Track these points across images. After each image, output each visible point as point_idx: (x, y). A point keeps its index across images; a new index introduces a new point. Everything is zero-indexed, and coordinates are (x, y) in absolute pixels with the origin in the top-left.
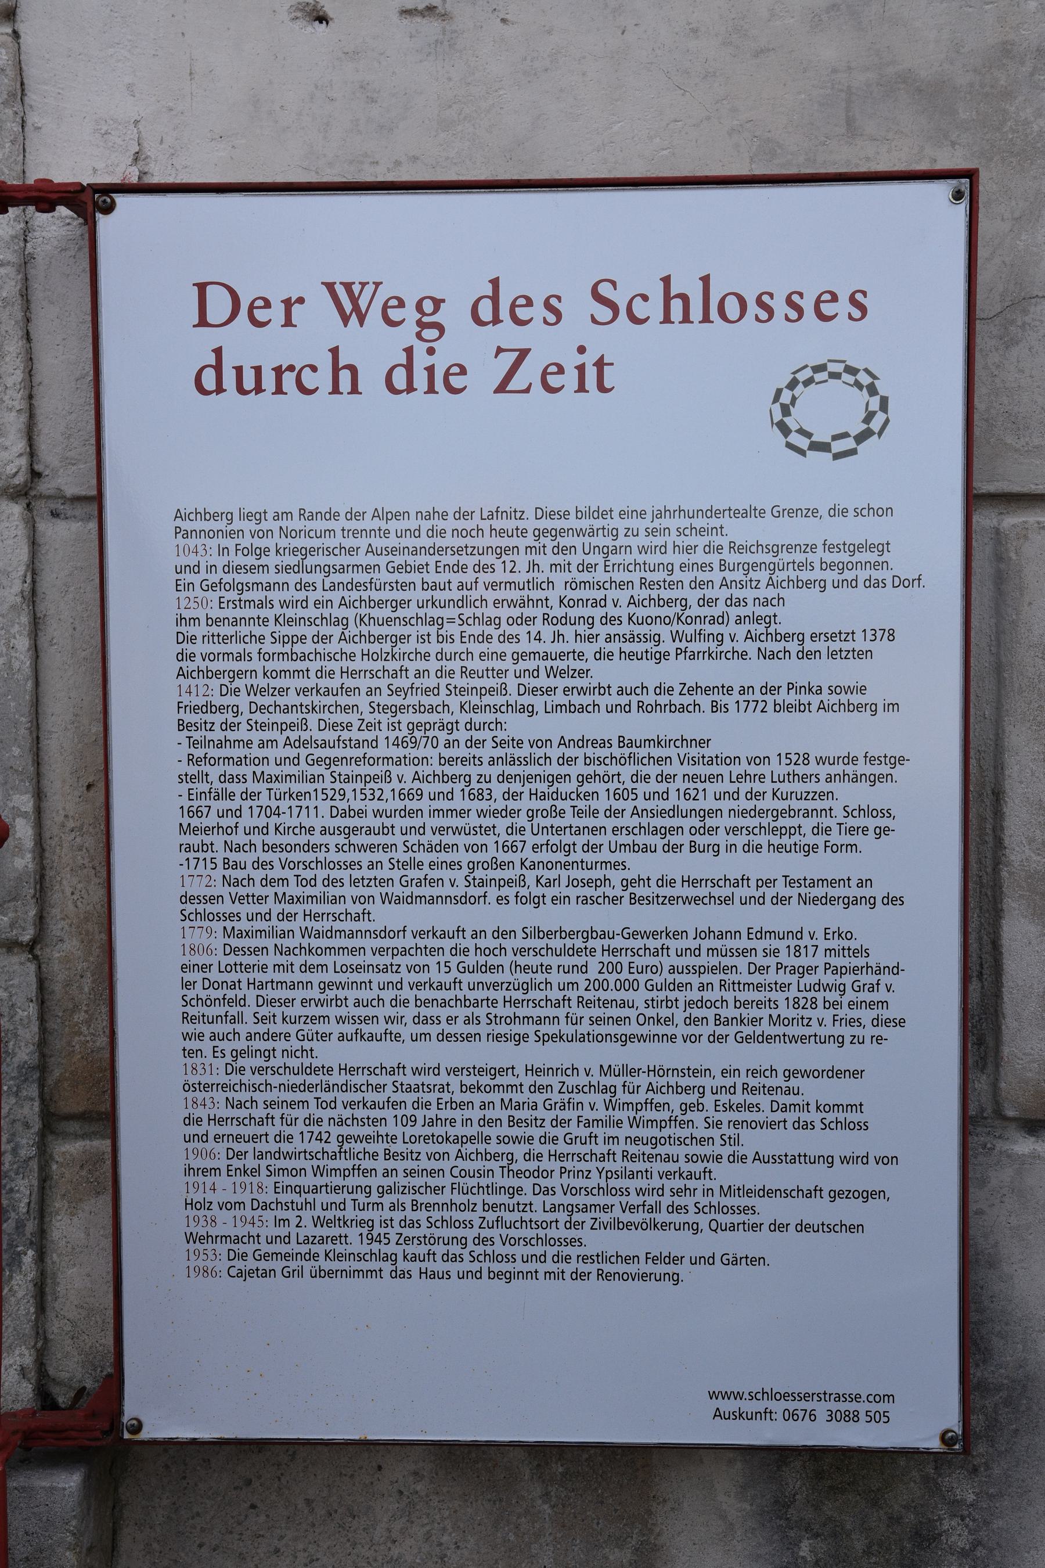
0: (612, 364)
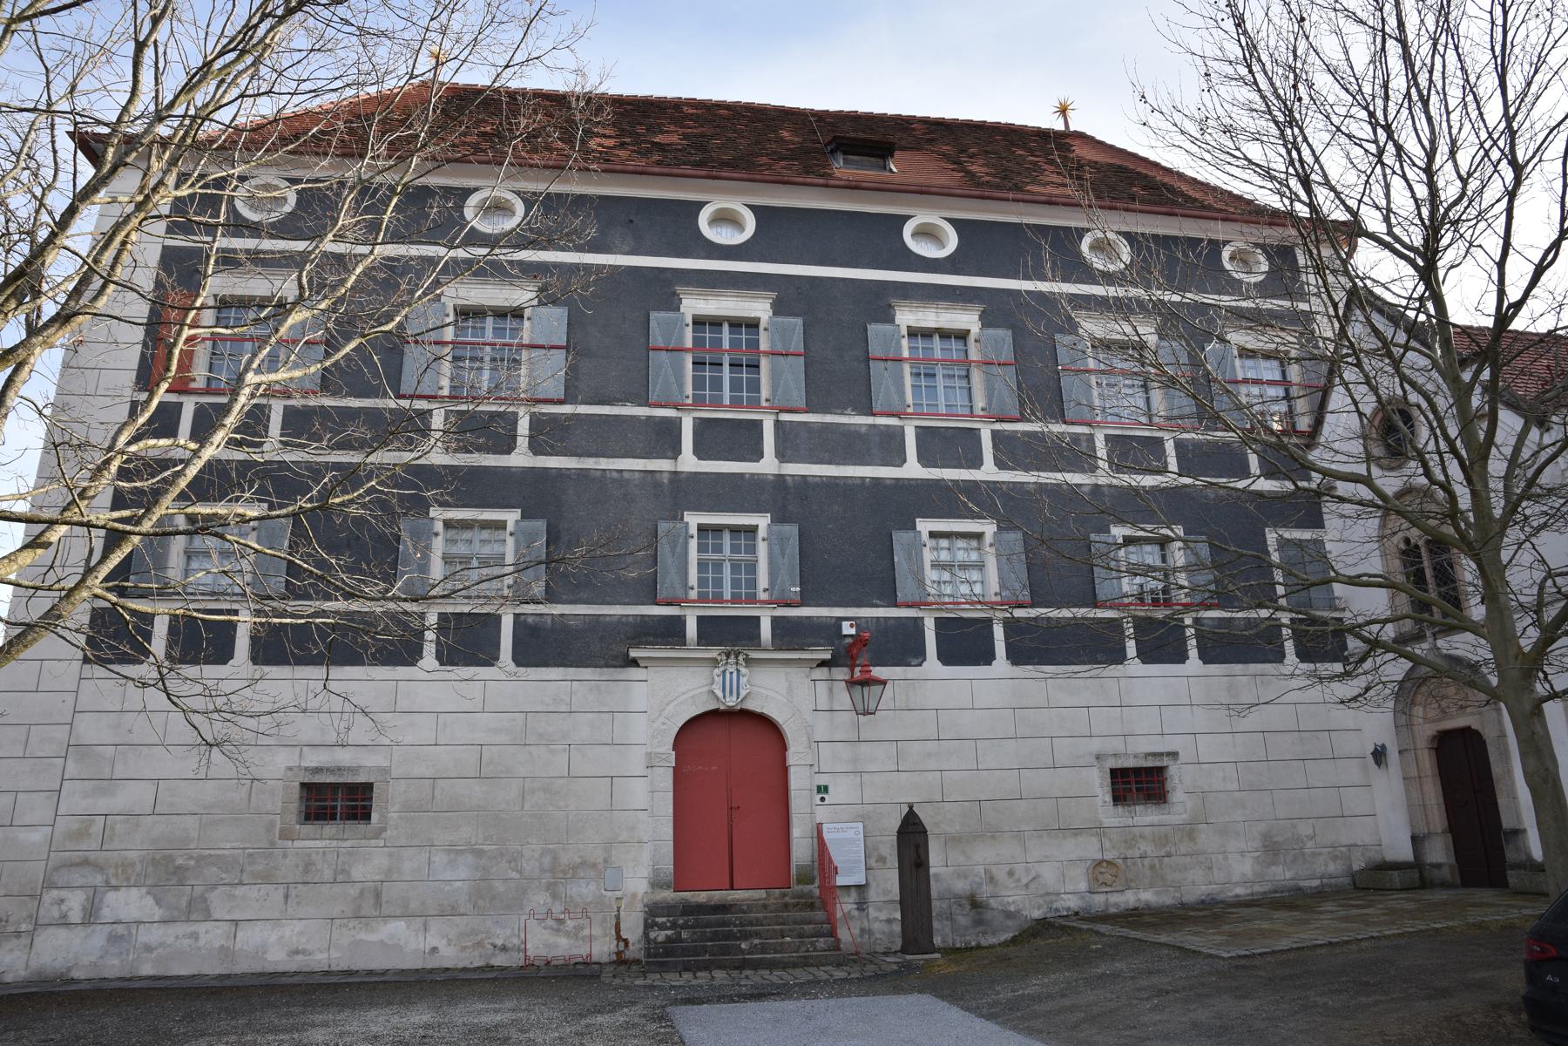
0: (912, 833)
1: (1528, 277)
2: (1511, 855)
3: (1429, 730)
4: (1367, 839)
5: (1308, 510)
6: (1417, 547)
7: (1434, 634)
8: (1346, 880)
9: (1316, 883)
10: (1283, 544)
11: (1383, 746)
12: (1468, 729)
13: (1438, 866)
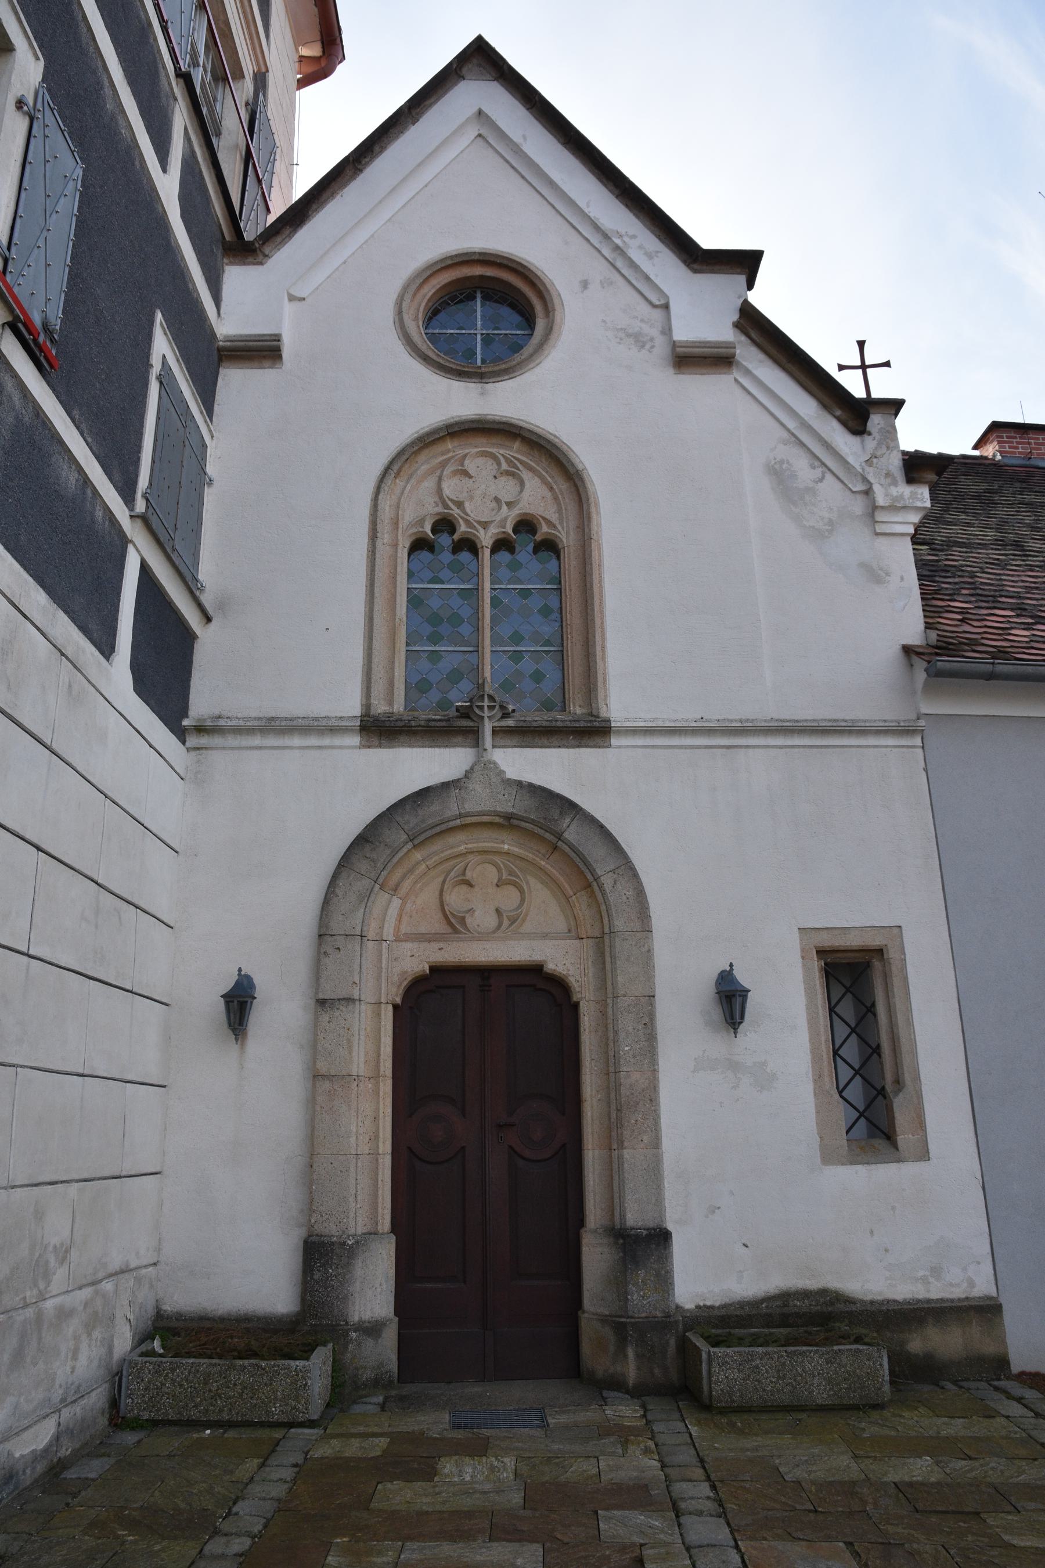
3: (415, 960)
12: (536, 970)
13: (373, 1329)
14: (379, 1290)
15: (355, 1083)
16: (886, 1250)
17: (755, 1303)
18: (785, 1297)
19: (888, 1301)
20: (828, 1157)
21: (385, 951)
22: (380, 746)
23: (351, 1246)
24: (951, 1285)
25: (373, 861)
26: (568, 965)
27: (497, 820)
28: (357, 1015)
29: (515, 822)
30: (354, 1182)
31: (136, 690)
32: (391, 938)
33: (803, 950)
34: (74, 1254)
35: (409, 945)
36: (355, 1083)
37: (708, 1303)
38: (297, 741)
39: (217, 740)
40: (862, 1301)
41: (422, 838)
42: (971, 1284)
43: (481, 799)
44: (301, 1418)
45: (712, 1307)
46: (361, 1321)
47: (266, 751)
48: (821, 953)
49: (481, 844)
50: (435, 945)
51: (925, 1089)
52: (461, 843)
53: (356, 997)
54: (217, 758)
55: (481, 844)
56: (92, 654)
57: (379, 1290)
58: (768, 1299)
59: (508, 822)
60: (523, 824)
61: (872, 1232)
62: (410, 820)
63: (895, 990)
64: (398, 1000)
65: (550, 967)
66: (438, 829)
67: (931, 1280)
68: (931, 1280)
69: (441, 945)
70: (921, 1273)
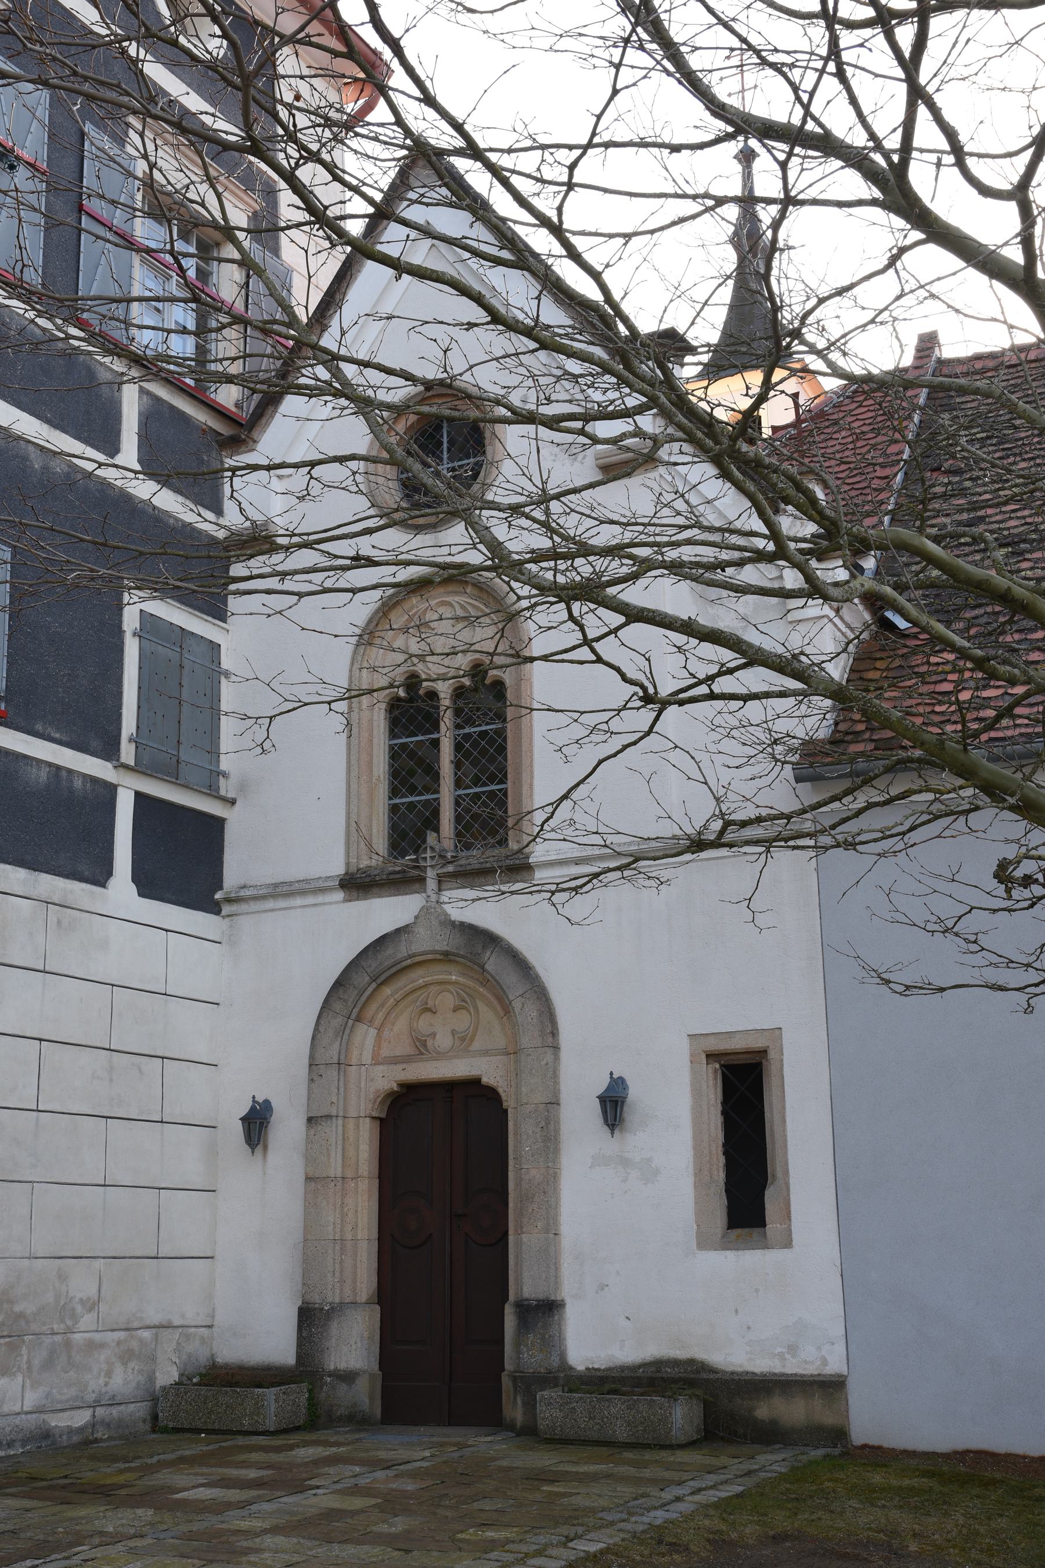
1: (986, 160)
2: (517, 1353)
3: (386, 1079)
4: (191, 1312)
5: (205, 572)
6: (433, 695)
7: (441, 880)
8: (138, 1410)
9: (81, 1418)
10: (149, 624)
11: (267, 1105)
12: (474, 1083)
13: (348, 1377)
14: (354, 1347)
15: (333, 1184)
16: (749, 1328)
17: (634, 1368)
18: (658, 1364)
19: (747, 1373)
20: (704, 1243)
21: (363, 1074)
22: (358, 899)
23: (328, 1311)
24: (806, 1362)
25: (345, 1001)
26: (498, 1078)
27: (438, 957)
28: (334, 1129)
29: (452, 957)
30: (331, 1261)
31: (141, 894)
32: (369, 1062)
33: (692, 1055)
34: (103, 1307)
35: (381, 1067)
36: (333, 1184)
37: (596, 1366)
38: (298, 901)
39: (243, 907)
40: (724, 1372)
41: (383, 978)
42: (824, 1362)
43: (425, 941)
44: (261, 1429)
45: (598, 1370)
46: (336, 1369)
47: (278, 912)
48: (711, 1056)
49: (435, 977)
50: (400, 1067)
51: (792, 1181)
52: (419, 977)
53: (334, 1113)
54: (245, 923)
55: (435, 977)
56: (83, 890)
57: (354, 1347)
58: (644, 1365)
59: (447, 957)
60: (458, 959)
61: (736, 1311)
62: (372, 965)
63: (773, 1088)
64: (383, 1115)
65: (485, 1080)
66: (394, 970)
67: (787, 1356)
68: (787, 1356)
69: (404, 1066)
70: (779, 1350)
